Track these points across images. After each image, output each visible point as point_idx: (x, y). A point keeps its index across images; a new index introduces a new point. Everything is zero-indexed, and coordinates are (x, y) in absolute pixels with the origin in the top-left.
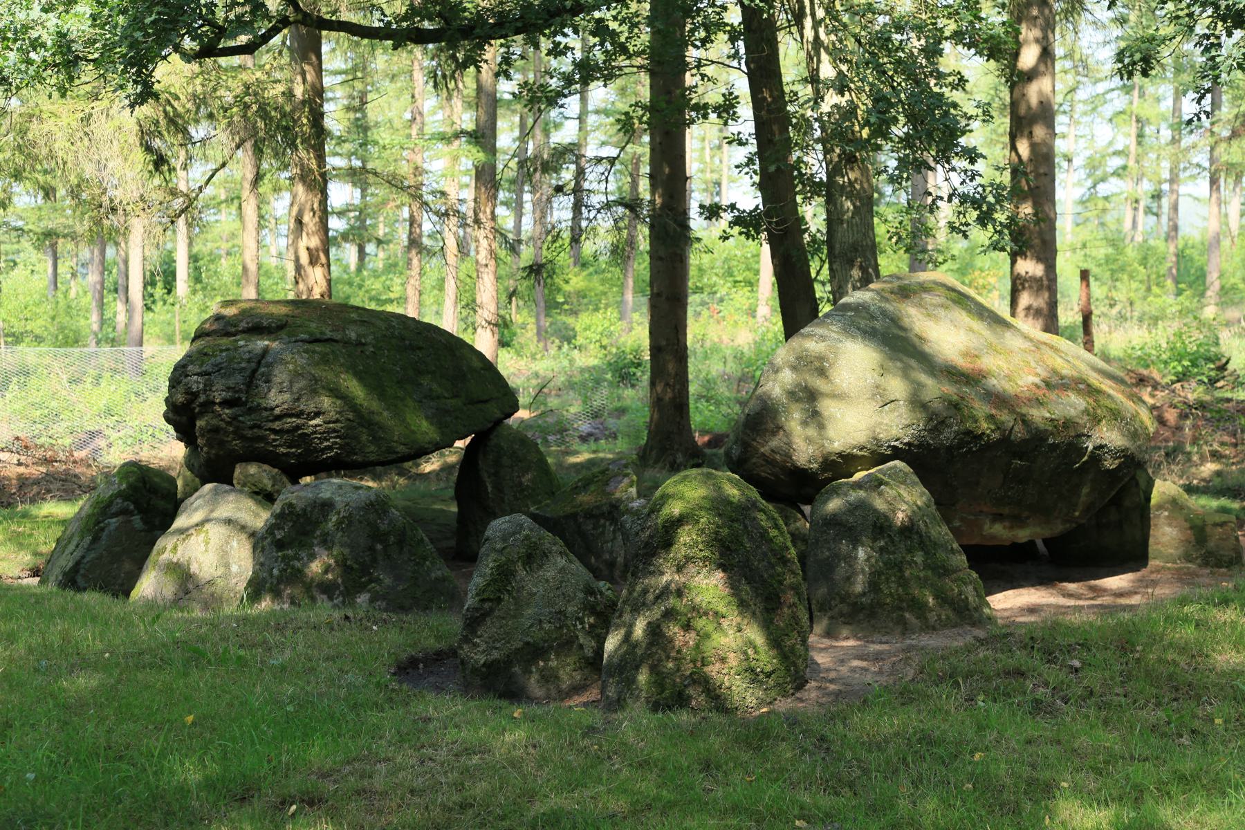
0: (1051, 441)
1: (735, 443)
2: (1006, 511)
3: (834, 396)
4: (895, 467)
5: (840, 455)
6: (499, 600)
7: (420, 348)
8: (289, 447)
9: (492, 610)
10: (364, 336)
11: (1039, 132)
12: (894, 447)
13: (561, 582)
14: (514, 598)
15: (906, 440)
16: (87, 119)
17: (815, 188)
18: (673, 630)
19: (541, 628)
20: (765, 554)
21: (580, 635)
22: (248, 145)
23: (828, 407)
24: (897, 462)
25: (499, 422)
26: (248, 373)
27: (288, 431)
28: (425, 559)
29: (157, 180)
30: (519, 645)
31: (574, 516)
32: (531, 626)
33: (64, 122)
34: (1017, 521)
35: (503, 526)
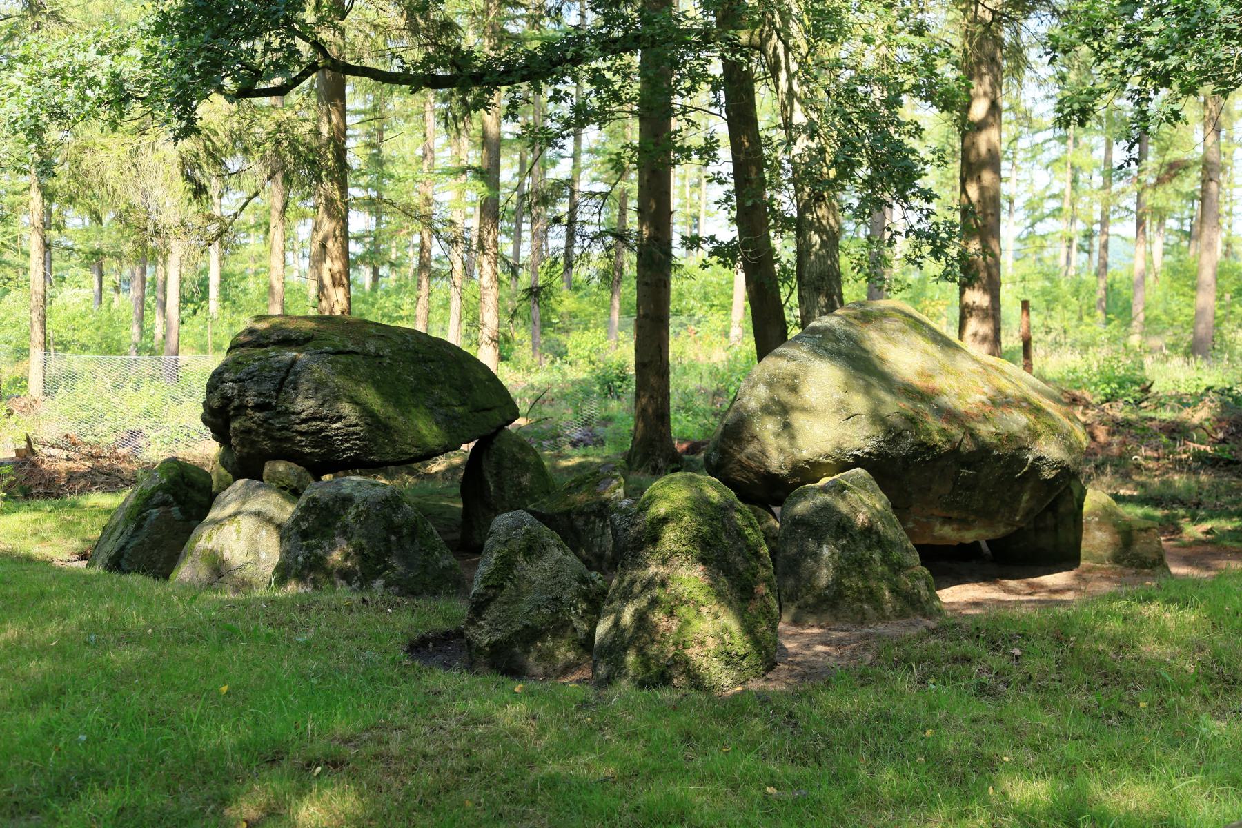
0: (995, 453)
1: (714, 450)
2: (955, 515)
3: (804, 410)
5: (808, 462)
6: (502, 587)
9: (495, 596)
11: (987, 177)
12: (856, 456)
15: (867, 450)
16: (135, 152)
17: (786, 223)
18: (658, 617)
19: (540, 613)
22: (279, 176)
23: (798, 419)
24: (859, 469)
25: (501, 428)
26: (277, 381)
28: (434, 549)
29: (195, 207)
33: (115, 152)
34: (965, 524)
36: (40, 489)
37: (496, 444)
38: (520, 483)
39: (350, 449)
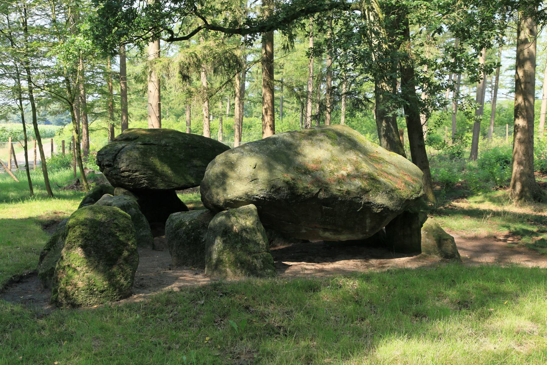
0: (340, 199)
2: (329, 227)
5: (231, 200)
11: (528, 66)
12: (256, 198)
15: (262, 196)
26: (114, 155)
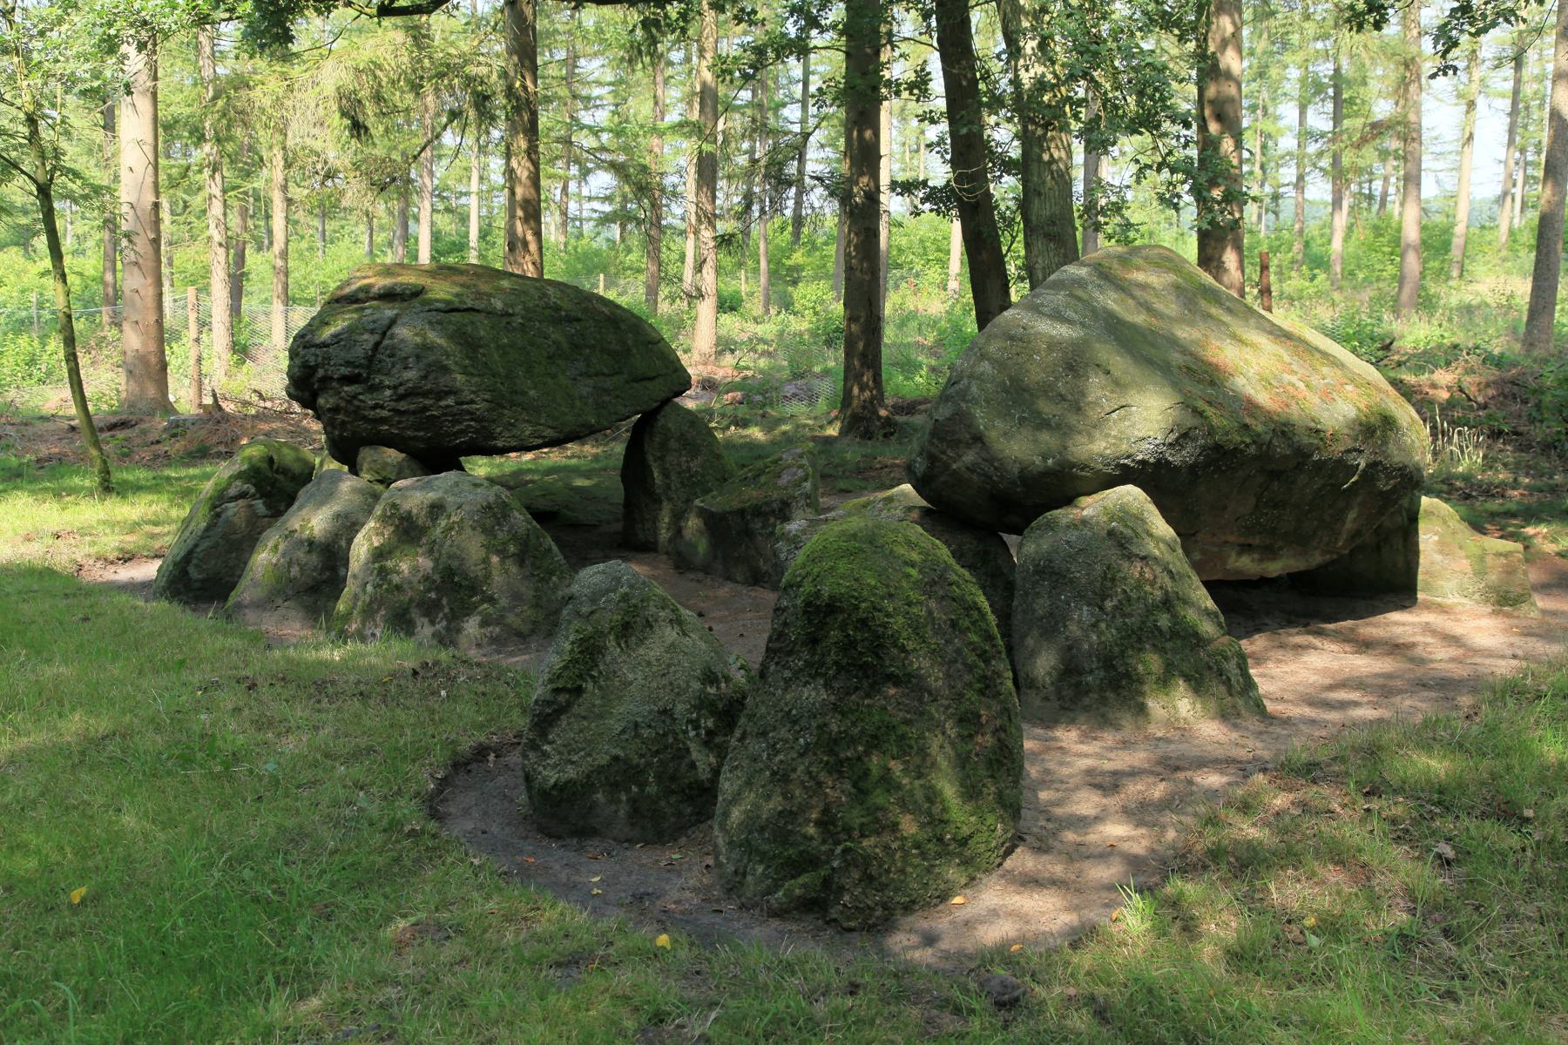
0: (1316, 457)
1: (920, 454)
2: (1256, 541)
4: (1128, 493)
6: (579, 691)
7: (578, 320)
8: (418, 430)
9: (569, 705)
10: (512, 306)
13: (669, 666)
14: (600, 688)
15: (1140, 457)
17: (1008, 166)
19: (637, 735)
20: (958, 651)
21: (693, 746)
24: (1130, 487)
25: (667, 401)
27: (414, 413)
28: (551, 573)
30: (603, 760)
31: (742, 512)
32: (623, 732)
34: (1269, 552)
35: (595, 580)
36: (222, 449)
37: (661, 421)
38: (689, 469)
39: (461, 432)
